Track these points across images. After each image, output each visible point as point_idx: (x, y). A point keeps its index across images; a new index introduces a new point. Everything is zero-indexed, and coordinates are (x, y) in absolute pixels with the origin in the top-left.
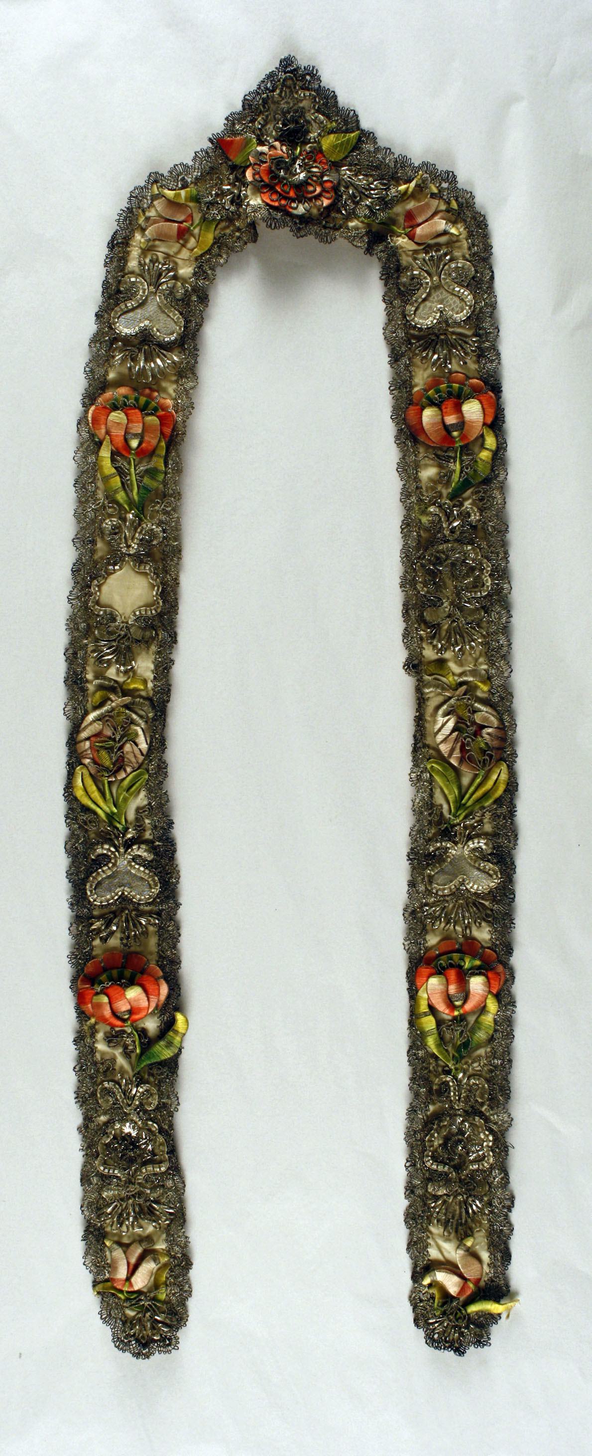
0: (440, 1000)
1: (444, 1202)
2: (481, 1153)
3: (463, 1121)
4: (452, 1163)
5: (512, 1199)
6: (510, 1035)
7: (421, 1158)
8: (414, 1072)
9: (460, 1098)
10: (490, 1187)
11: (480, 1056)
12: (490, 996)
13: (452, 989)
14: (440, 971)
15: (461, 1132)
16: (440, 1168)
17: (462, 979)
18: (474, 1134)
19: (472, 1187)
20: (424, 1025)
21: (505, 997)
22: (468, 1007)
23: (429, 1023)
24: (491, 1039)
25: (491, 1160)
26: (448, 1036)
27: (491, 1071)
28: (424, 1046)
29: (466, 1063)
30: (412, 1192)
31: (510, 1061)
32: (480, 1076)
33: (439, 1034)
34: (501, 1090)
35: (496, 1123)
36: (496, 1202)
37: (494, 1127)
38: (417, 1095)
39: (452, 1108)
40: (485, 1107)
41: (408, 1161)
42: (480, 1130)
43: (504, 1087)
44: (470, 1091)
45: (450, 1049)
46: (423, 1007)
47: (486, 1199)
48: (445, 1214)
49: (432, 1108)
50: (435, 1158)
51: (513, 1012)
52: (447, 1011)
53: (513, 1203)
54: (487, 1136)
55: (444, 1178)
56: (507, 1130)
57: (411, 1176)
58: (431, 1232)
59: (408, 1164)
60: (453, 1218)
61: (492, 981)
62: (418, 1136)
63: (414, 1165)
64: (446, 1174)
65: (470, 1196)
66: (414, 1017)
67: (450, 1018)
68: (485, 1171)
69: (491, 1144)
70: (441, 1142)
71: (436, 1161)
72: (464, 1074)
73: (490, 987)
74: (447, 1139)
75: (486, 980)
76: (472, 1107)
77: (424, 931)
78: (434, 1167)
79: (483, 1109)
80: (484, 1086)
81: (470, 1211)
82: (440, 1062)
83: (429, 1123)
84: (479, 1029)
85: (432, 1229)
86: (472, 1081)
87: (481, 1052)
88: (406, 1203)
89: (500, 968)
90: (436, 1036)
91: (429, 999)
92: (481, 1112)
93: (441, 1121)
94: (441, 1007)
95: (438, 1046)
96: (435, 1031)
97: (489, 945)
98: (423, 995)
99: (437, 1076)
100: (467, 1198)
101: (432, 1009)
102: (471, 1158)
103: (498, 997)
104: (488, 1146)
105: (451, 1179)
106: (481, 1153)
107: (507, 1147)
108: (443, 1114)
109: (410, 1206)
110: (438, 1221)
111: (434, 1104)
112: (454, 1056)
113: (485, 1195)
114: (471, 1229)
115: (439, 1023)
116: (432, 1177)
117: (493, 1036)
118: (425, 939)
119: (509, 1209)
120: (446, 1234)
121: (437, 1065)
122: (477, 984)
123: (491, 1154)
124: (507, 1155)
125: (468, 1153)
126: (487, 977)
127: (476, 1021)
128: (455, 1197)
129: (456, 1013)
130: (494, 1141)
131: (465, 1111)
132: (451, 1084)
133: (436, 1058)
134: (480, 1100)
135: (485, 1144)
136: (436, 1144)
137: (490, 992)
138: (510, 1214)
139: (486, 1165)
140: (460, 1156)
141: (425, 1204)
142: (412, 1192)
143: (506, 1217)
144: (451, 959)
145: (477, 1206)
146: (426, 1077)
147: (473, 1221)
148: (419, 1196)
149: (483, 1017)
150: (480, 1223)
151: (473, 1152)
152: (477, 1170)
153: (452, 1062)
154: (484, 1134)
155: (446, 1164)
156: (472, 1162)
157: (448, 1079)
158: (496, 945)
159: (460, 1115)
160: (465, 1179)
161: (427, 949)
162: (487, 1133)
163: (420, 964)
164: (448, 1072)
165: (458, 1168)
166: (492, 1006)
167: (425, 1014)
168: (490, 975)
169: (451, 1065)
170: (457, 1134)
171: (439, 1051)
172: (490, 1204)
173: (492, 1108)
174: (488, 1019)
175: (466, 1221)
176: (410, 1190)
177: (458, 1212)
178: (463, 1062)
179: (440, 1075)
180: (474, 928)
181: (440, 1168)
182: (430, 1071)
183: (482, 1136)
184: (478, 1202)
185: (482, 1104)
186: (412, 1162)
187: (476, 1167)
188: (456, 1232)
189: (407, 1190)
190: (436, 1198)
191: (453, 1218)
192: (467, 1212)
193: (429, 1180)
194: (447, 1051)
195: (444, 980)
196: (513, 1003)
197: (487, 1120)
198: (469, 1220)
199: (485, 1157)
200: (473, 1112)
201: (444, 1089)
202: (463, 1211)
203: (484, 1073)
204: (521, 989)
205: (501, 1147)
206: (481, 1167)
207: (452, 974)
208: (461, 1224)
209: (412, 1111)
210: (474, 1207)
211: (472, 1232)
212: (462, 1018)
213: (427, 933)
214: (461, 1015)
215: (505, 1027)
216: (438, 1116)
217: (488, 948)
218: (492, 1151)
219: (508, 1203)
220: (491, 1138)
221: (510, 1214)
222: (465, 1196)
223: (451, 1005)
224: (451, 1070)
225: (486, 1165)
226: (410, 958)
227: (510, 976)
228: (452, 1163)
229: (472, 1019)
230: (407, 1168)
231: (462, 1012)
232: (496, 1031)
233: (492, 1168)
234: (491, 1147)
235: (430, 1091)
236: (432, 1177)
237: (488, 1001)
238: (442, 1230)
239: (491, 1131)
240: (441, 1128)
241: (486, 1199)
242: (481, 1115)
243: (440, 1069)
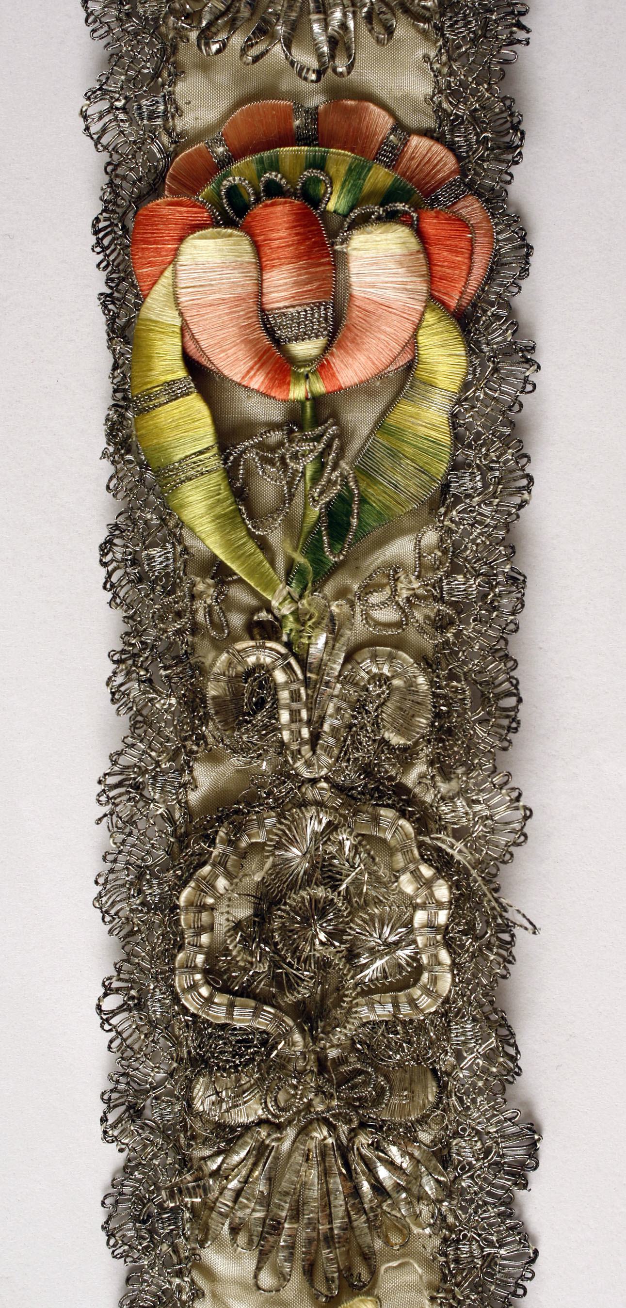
0: (231, 332)
1: (261, 1151)
2: (403, 954)
3: (332, 827)
4: (290, 998)
5: (531, 1135)
6: (512, 481)
7: (166, 978)
8: (134, 627)
9: (315, 738)
10: (442, 1088)
11: (393, 571)
12: (430, 318)
13: (282, 286)
14: (233, 213)
15: (325, 872)
16: (242, 1018)
17: (320, 243)
18: (376, 879)
19: (368, 1091)
20: (169, 437)
21: (487, 322)
22: (351, 369)
23: (185, 427)
24: (443, 497)
25: (445, 984)
26: (267, 486)
27: (441, 624)
28: (172, 529)
29: (342, 593)
30: (135, 1112)
31: (517, 581)
32: (399, 644)
33: (230, 474)
34: (483, 700)
35: (459, 834)
36: (466, 1150)
37: (457, 850)
38: (141, 722)
39: (285, 774)
40: (420, 768)
41: (108, 991)
42: (399, 860)
43: (491, 683)
44: (360, 707)
45: (276, 537)
46: (166, 364)
47: (425, 1137)
48: (266, 1201)
49: (206, 778)
50: (217, 975)
51: (528, 386)
52: (257, 382)
53: (533, 1149)
54: (428, 884)
55: (253, 1056)
56: (506, 857)
57: (124, 1051)
58: (208, 1273)
59: (111, 1003)
60: (296, 1214)
61: (441, 254)
62: (153, 892)
63: (137, 1004)
64: (267, 1042)
65: (363, 1125)
66: (125, 431)
67: (272, 412)
68: (421, 1028)
69: (442, 917)
70: (243, 912)
71: (225, 990)
72: (335, 634)
73: (431, 278)
74: (266, 901)
75: (413, 243)
76: (367, 770)
77: (169, 63)
78: (218, 1014)
79: (410, 779)
80: (411, 684)
81: (366, 1187)
82: (238, 594)
83: (194, 837)
84: (394, 455)
85: (212, 1256)
86: (367, 667)
87: (402, 548)
88: (112, 1158)
89: (471, 208)
90: (216, 480)
91: (184, 329)
92: (401, 789)
93: (239, 829)
94: (233, 362)
95: (226, 522)
96: (212, 460)
97: (429, 122)
98: (157, 307)
99: (219, 646)
100: (353, 1133)
101: (200, 375)
102: (369, 973)
103: (465, 321)
104: (430, 925)
105: (283, 1063)
106: (403, 954)
107: (507, 927)
108: (251, 800)
109: (127, 1169)
110: (234, 1230)
111: (213, 758)
112: (290, 564)
113: (422, 1120)
114: (368, 1258)
115: (229, 434)
116: (208, 1053)
117: (446, 487)
118: (170, 99)
119: (520, 1174)
120: (266, 1279)
121: (227, 604)
122: (378, 260)
123: (444, 956)
124: (509, 960)
125: (351, 956)
126: (420, 233)
127: (380, 425)
128: (304, 1131)
129: (298, 392)
130: (457, 903)
131: (339, 789)
132: (280, 676)
133: (220, 573)
134: (396, 740)
135: (420, 917)
136: (222, 922)
137: (433, 300)
138: (521, 1194)
139: (424, 1002)
140: (324, 965)
141: (185, 1163)
142: (135, 1112)
143: (509, 1202)
144: (275, 165)
145: (391, 1164)
146: (179, 656)
147: (374, 1226)
148: (163, 1131)
149: (405, 410)
150: (404, 1230)
151: (374, 953)
152: (390, 1025)
153: (283, 590)
154: (416, 875)
155: (263, 999)
156: (368, 991)
157: (266, 659)
158: (456, 123)
159: (320, 804)
160: (341, 1061)
161: (180, 141)
162: (427, 871)
163: (141, 207)
164: (265, 630)
165: (312, 1017)
166: (444, 359)
167: (173, 391)
168: (431, 225)
169: (280, 602)
170: (308, 880)
171: (229, 545)
172: (442, 1155)
173: (446, 774)
174: (428, 419)
175: (349, 1226)
176: (126, 1104)
177: (315, 1193)
178: (329, 589)
179: (234, 638)
180: (366, 46)
181: (242, 1018)
182: (195, 629)
183: (407, 884)
184: (394, 1152)
185: (406, 757)
186: (137, 987)
187: (383, 1011)
188: (309, 1271)
189: (110, 1105)
190: (228, 1136)
191: (296, 1214)
192: (355, 1192)
193: (200, 1063)
194: (263, 545)
195: (246, 246)
196: (524, 354)
197: (426, 821)
198: (360, 1222)
199: (419, 970)
200: (372, 789)
201: (252, 698)
202: (336, 1183)
203: (412, 635)
204: (557, 300)
205: (484, 929)
206: (406, 1010)
207: (278, 220)
208: (329, 1239)
209: (125, 786)
210: (383, 1172)
211: (373, 1273)
212: (321, 412)
213: (178, 73)
214: (317, 400)
215: (493, 448)
216: (229, 811)
217: (426, 133)
218: (448, 944)
219: (515, 1153)
220: (442, 892)
221: (521, 1194)
222: (343, 1129)
223: (280, 365)
224: (281, 620)
225: (424, 1002)
226: (112, 169)
227: (515, 251)
228: (290, 998)
229: (361, 419)
230: (106, 1017)
231: (320, 387)
232: (455, 466)
233: (447, 1012)
234: (446, 930)
235: (194, 701)
236: (208, 1053)
237: (423, 339)
238: (250, 1264)
239: (444, 864)
240: (243, 855)
241: (425, 1137)
242: (404, 801)
243: (237, 620)
